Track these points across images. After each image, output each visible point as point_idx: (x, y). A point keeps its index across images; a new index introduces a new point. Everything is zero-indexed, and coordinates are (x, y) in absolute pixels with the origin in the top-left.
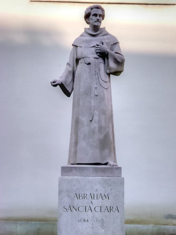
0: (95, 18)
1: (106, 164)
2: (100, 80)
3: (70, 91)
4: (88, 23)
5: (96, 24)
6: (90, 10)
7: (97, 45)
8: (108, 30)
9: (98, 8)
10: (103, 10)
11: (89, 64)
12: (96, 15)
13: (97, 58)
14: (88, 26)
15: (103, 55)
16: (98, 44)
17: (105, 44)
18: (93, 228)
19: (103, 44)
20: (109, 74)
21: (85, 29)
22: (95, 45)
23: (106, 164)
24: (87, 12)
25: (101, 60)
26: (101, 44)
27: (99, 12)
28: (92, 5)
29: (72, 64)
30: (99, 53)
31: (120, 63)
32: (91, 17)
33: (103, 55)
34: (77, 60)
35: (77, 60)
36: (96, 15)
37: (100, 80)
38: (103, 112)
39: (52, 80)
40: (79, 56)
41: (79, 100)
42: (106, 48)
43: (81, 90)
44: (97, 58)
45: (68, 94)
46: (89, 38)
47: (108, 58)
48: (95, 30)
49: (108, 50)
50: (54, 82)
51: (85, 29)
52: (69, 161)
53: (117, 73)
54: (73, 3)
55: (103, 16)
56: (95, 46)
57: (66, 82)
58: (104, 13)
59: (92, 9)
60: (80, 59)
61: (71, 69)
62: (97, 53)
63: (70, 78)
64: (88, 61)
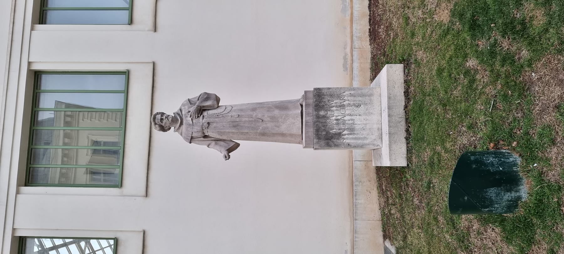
0: (164, 121)
1: (302, 106)
2: (224, 113)
3: (233, 144)
4: (170, 129)
5: (170, 119)
6: (157, 126)
7: (191, 116)
8: (176, 110)
9: (154, 118)
10: (157, 114)
11: (209, 123)
12: (162, 119)
13: (203, 117)
14: (172, 128)
15: (201, 111)
16: (189, 116)
17: (190, 110)
18: (360, 115)
19: (189, 112)
20: (218, 107)
21: (175, 131)
22: (190, 119)
23: (302, 106)
24: (158, 128)
25: (205, 113)
26: (190, 113)
27: (159, 117)
28: (153, 123)
29: (209, 142)
30: (198, 114)
31: (207, 97)
32: (163, 124)
33: (201, 111)
34: (205, 137)
35: (205, 137)
36: (162, 119)
37: (224, 113)
38: (254, 110)
39: (224, 159)
40: (200, 134)
41: (242, 133)
42: (193, 109)
43: (233, 131)
44: (203, 117)
45: (237, 145)
46: (184, 127)
47: (203, 107)
48: (178, 120)
49: (195, 106)
50: (226, 157)
51: (175, 131)
52: (299, 143)
53: (218, 100)
54: (151, 156)
55: (163, 114)
56: (192, 119)
57: (225, 147)
58: (160, 113)
59: (155, 124)
60: (204, 133)
61: (213, 143)
62: (198, 117)
63: (222, 143)
64: (206, 125)
